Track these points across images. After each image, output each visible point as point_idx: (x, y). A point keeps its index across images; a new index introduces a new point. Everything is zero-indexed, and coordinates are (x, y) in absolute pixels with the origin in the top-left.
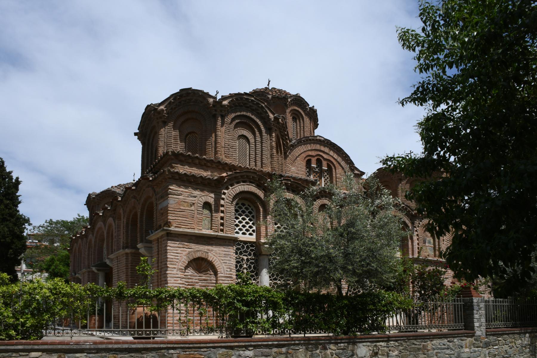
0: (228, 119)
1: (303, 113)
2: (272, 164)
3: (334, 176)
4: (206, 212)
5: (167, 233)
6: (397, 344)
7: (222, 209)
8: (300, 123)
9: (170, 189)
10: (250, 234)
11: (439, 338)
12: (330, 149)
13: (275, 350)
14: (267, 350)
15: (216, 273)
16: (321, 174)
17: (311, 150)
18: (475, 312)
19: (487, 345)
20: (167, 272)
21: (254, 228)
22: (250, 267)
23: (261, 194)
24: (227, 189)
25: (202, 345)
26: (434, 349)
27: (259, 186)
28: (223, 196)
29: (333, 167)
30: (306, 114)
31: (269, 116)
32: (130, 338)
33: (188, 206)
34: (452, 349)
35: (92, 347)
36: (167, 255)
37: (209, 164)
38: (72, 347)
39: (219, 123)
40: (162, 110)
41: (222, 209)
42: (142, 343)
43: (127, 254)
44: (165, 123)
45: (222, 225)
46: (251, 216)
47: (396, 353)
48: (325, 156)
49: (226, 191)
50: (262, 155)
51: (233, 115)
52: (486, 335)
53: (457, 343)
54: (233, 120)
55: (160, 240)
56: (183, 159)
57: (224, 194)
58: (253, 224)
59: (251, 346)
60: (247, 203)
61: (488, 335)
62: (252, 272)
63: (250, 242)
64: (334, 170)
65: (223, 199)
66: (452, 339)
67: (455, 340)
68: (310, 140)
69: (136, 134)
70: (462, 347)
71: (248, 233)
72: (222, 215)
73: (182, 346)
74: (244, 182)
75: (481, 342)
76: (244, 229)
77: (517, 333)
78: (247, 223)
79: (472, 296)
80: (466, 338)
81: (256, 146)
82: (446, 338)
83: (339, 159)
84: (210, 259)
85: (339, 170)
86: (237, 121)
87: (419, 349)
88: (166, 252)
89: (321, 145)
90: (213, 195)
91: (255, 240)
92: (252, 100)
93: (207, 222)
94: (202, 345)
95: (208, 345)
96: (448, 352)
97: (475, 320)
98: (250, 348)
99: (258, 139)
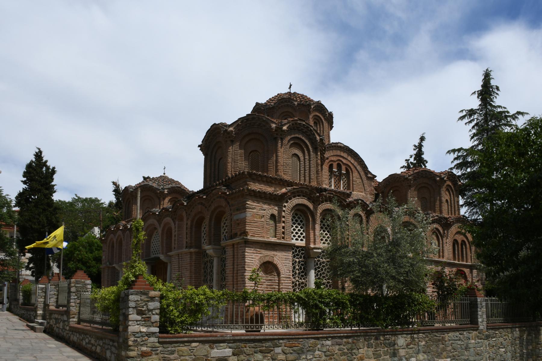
0: (285, 141)
1: (323, 119)
2: (317, 179)
3: (351, 179)
4: (272, 222)
5: (245, 241)
6: (424, 336)
7: (283, 219)
8: (320, 127)
9: (247, 204)
10: (302, 240)
11: (453, 331)
12: (349, 155)
13: (345, 340)
14: (340, 340)
15: (279, 274)
16: (339, 176)
17: (333, 156)
18: (479, 309)
19: (487, 337)
20: (246, 274)
21: (304, 234)
22: (301, 268)
23: (311, 206)
24: (287, 202)
25: (300, 337)
26: (450, 340)
27: (309, 199)
28: (284, 209)
29: (350, 171)
30: (325, 119)
31: (316, 138)
32: (243, 331)
33: (259, 218)
34: (462, 341)
35: (231, 338)
36: (245, 260)
37: (273, 181)
38: (218, 339)
39: (279, 145)
40: (232, 131)
41: (283, 219)
42: (253, 335)
43: (191, 253)
44: (232, 142)
45: (283, 233)
46: (302, 224)
47: (424, 343)
48: (344, 161)
49: (286, 204)
50: (310, 171)
51: (289, 137)
52: (487, 329)
53: (466, 335)
54: (289, 141)
55: (235, 246)
56: (255, 177)
57: (285, 206)
58: (303, 231)
59: (330, 337)
60: (299, 213)
61: (490, 329)
62: (302, 272)
63: (301, 247)
64: (351, 174)
65: (284, 211)
66: (462, 332)
67: (465, 333)
68: (333, 146)
69: (199, 146)
70: (469, 339)
71: (300, 239)
72: (283, 225)
73: (288, 337)
74: (299, 196)
75: (483, 335)
76: (297, 236)
77: (509, 328)
78: (299, 230)
79: (476, 296)
80: (472, 332)
81: (305, 164)
82: (458, 331)
83: (356, 164)
84: (275, 262)
85: (356, 174)
86: (292, 142)
87: (439, 340)
88: (244, 257)
89: (341, 151)
90: (276, 208)
91: (304, 245)
92: (304, 125)
93: (272, 231)
94: (300, 337)
95: (304, 336)
96: (459, 342)
97: (479, 317)
98: (330, 339)
99: (307, 157)
